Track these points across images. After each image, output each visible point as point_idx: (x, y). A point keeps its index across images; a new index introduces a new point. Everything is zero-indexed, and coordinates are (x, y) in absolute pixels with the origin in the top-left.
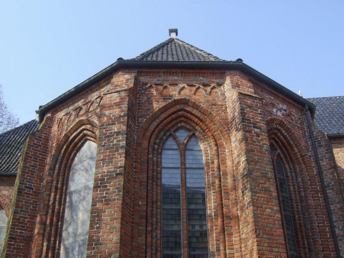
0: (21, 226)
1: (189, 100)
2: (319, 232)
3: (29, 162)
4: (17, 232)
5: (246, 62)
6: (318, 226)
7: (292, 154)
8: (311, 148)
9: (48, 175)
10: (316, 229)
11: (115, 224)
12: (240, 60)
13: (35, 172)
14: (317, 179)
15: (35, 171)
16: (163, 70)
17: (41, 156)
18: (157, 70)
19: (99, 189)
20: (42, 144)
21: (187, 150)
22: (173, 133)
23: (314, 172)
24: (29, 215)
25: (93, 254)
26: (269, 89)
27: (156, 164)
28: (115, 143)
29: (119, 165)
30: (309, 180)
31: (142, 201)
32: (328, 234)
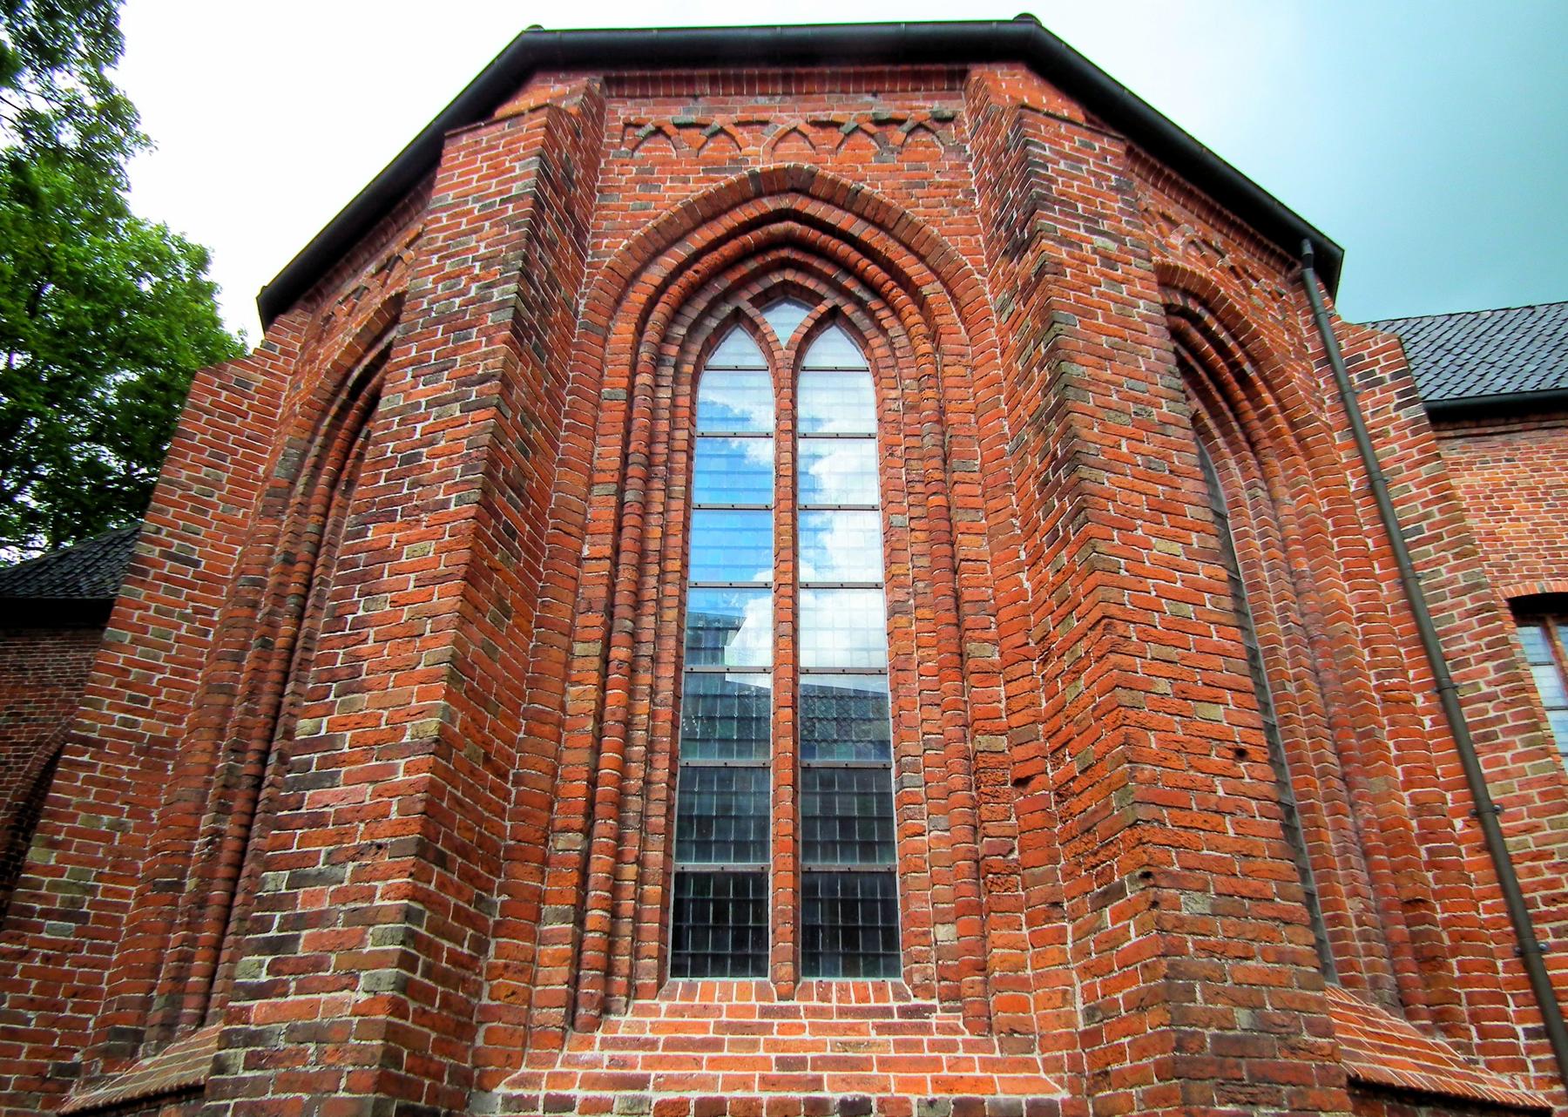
1: (812, 175)
7: (1252, 415)
8: (1331, 398)
10: (1371, 699)
11: (435, 599)
12: (1026, 18)
14: (1362, 510)
16: (707, 72)
17: (241, 450)
18: (684, 72)
20: (251, 407)
21: (804, 369)
22: (751, 311)
23: (1347, 485)
25: (323, 732)
27: (666, 414)
28: (473, 293)
32: (1427, 721)
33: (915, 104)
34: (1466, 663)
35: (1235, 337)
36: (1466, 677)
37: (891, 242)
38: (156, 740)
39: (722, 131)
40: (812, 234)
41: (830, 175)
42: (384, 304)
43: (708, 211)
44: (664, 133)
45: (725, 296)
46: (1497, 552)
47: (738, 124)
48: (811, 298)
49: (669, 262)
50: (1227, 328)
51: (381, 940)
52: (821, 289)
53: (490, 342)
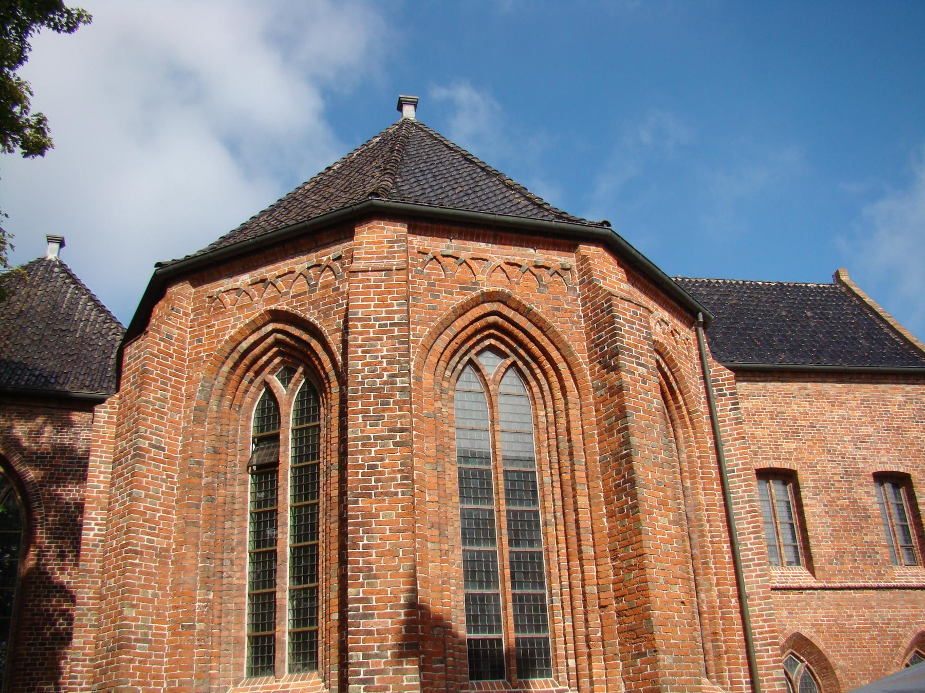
0: (150, 528)
2: (713, 552)
3: (152, 391)
4: (142, 539)
5: (616, 228)
6: (711, 542)
9: (194, 421)
13: (166, 414)
15: (166, 410)
19: (361, 471)
20: (174, 351)
22: (474, 358)
24: (161, 505)
26: (646, 282)
28: (385, 378)
29: (399, 425)
30: (699, 457)
31: (430, 495)
33: (554, 258)
34: (744, 534)
35: (670, 370)
36: (743, 540)
37: (544, 337)
38: (163, 549)
39: (465, 261)
40: (506, 324)
41: (518, 298)
42: (266, 311)
43: (462, 311)
44: (437, 260)
45: (465, 354)
46: (754, 444)
47: (473, 259)
48: (504, 355)
49: (445, 338)
50: (668, 365)
51: (411, 680)
52: (508, 351)
53: (401, 410)
